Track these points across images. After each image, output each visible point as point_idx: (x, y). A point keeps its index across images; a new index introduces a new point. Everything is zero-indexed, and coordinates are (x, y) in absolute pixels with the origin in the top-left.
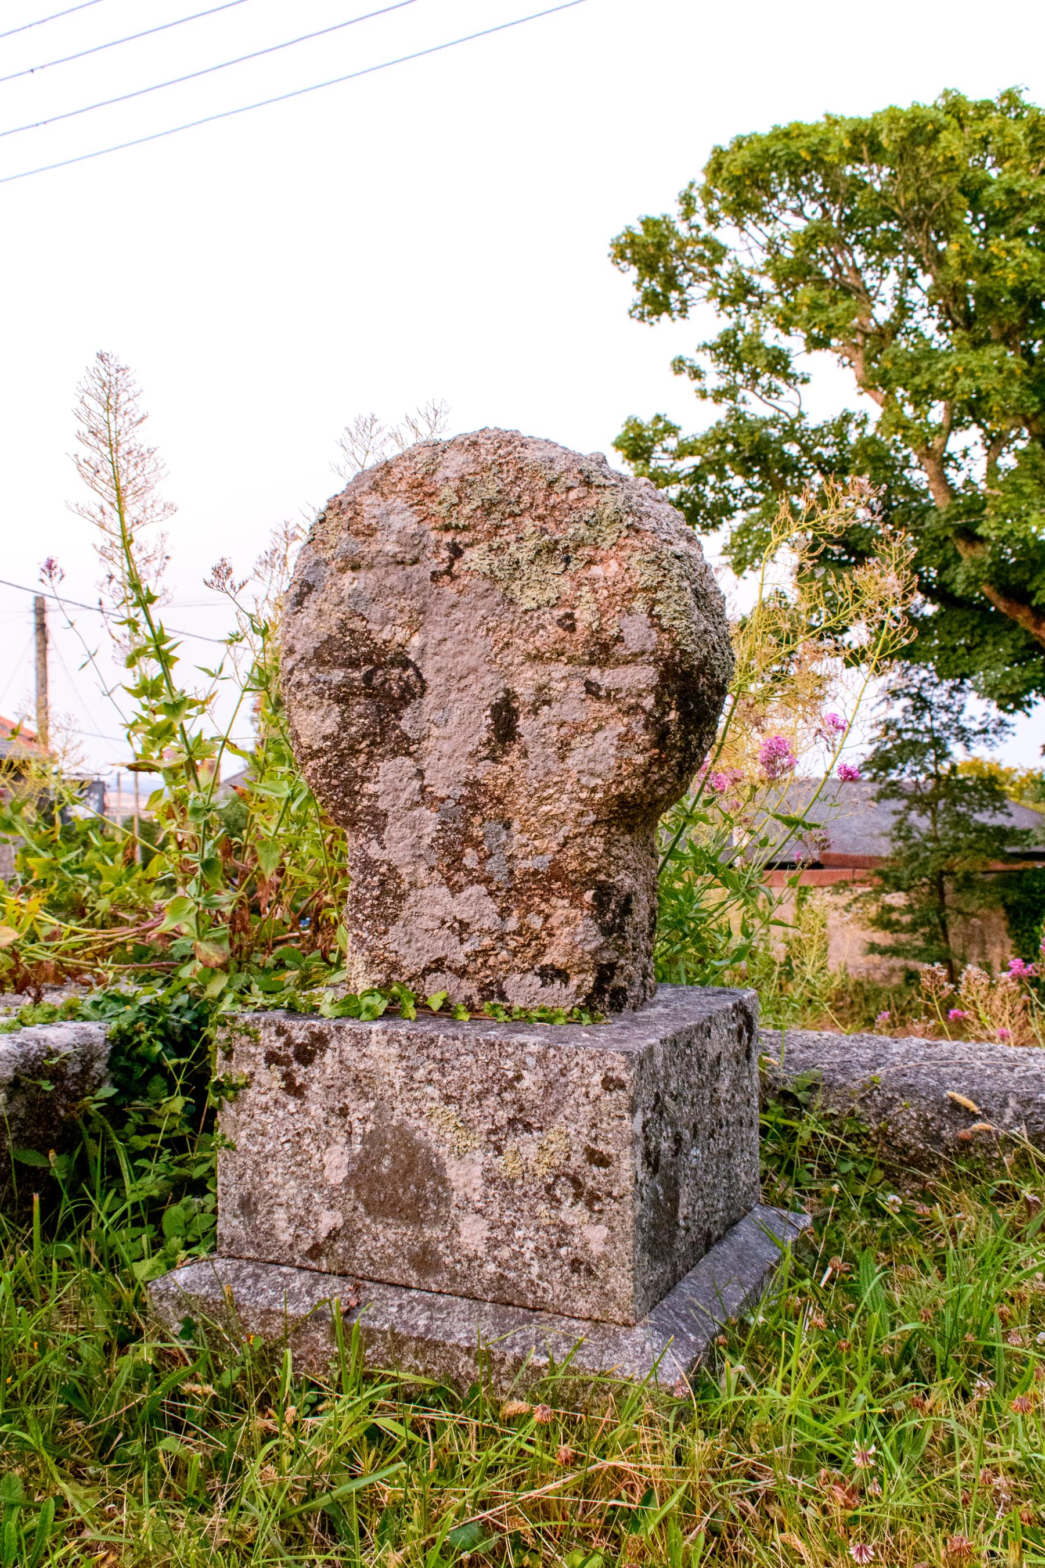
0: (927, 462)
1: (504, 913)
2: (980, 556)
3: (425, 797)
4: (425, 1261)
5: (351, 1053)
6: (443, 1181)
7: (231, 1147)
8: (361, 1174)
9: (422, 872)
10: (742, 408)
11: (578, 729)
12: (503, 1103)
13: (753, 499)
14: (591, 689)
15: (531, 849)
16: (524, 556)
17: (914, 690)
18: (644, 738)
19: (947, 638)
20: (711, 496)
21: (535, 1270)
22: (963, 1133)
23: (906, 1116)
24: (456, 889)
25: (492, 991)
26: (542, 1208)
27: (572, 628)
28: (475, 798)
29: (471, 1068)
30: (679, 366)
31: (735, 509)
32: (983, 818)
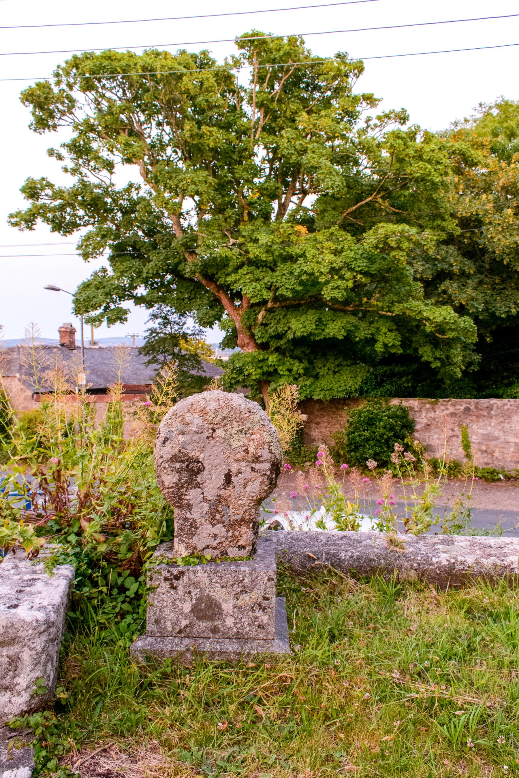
0: (173, 216)
1: (228, 531)
2: (196, 261)
3: (205, 500)
4: (215, 630)
5: (192, 576)
6: (221, 609)
7: (152, 605)
8: (195, 610)
9: (203, 521)
10: (85, 179)
11: (249, 480)
12: (239, 587)
13: (88, 221)
14: (253, 469)
15: (234, 513)
16: (234, 432)
17: (163, 315)
18: (267, 482)
19: (180, 295)
20: (68, 218)
21: (248, 629)
22: (313, 565)
23: (296, 560)
24: (214, 525)
25: (224, 553)
26: (250, 613)
27: (248, 453)
28: (219, 500)
29: (229, 578)
30: (51, 152)
31: (80, 225)
32: (194, 372)
